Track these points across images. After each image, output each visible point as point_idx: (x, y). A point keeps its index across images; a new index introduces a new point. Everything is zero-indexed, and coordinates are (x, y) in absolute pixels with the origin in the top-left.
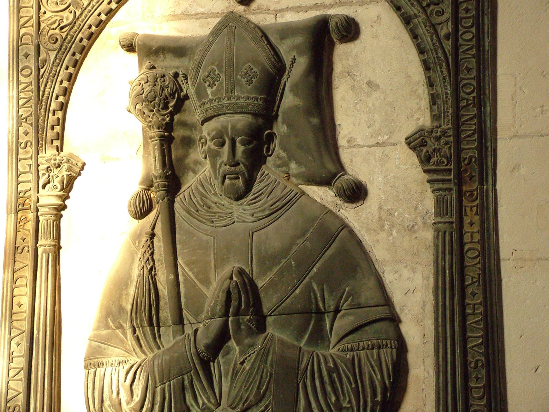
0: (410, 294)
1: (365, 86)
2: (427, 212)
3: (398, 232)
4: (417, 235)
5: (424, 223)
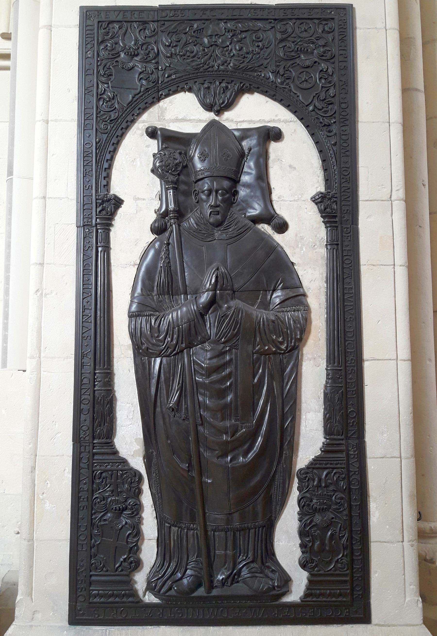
0: (313, 282)
1: (288, 168)
2: (322, 238)
3: (306, 248)
5: (320, 244)
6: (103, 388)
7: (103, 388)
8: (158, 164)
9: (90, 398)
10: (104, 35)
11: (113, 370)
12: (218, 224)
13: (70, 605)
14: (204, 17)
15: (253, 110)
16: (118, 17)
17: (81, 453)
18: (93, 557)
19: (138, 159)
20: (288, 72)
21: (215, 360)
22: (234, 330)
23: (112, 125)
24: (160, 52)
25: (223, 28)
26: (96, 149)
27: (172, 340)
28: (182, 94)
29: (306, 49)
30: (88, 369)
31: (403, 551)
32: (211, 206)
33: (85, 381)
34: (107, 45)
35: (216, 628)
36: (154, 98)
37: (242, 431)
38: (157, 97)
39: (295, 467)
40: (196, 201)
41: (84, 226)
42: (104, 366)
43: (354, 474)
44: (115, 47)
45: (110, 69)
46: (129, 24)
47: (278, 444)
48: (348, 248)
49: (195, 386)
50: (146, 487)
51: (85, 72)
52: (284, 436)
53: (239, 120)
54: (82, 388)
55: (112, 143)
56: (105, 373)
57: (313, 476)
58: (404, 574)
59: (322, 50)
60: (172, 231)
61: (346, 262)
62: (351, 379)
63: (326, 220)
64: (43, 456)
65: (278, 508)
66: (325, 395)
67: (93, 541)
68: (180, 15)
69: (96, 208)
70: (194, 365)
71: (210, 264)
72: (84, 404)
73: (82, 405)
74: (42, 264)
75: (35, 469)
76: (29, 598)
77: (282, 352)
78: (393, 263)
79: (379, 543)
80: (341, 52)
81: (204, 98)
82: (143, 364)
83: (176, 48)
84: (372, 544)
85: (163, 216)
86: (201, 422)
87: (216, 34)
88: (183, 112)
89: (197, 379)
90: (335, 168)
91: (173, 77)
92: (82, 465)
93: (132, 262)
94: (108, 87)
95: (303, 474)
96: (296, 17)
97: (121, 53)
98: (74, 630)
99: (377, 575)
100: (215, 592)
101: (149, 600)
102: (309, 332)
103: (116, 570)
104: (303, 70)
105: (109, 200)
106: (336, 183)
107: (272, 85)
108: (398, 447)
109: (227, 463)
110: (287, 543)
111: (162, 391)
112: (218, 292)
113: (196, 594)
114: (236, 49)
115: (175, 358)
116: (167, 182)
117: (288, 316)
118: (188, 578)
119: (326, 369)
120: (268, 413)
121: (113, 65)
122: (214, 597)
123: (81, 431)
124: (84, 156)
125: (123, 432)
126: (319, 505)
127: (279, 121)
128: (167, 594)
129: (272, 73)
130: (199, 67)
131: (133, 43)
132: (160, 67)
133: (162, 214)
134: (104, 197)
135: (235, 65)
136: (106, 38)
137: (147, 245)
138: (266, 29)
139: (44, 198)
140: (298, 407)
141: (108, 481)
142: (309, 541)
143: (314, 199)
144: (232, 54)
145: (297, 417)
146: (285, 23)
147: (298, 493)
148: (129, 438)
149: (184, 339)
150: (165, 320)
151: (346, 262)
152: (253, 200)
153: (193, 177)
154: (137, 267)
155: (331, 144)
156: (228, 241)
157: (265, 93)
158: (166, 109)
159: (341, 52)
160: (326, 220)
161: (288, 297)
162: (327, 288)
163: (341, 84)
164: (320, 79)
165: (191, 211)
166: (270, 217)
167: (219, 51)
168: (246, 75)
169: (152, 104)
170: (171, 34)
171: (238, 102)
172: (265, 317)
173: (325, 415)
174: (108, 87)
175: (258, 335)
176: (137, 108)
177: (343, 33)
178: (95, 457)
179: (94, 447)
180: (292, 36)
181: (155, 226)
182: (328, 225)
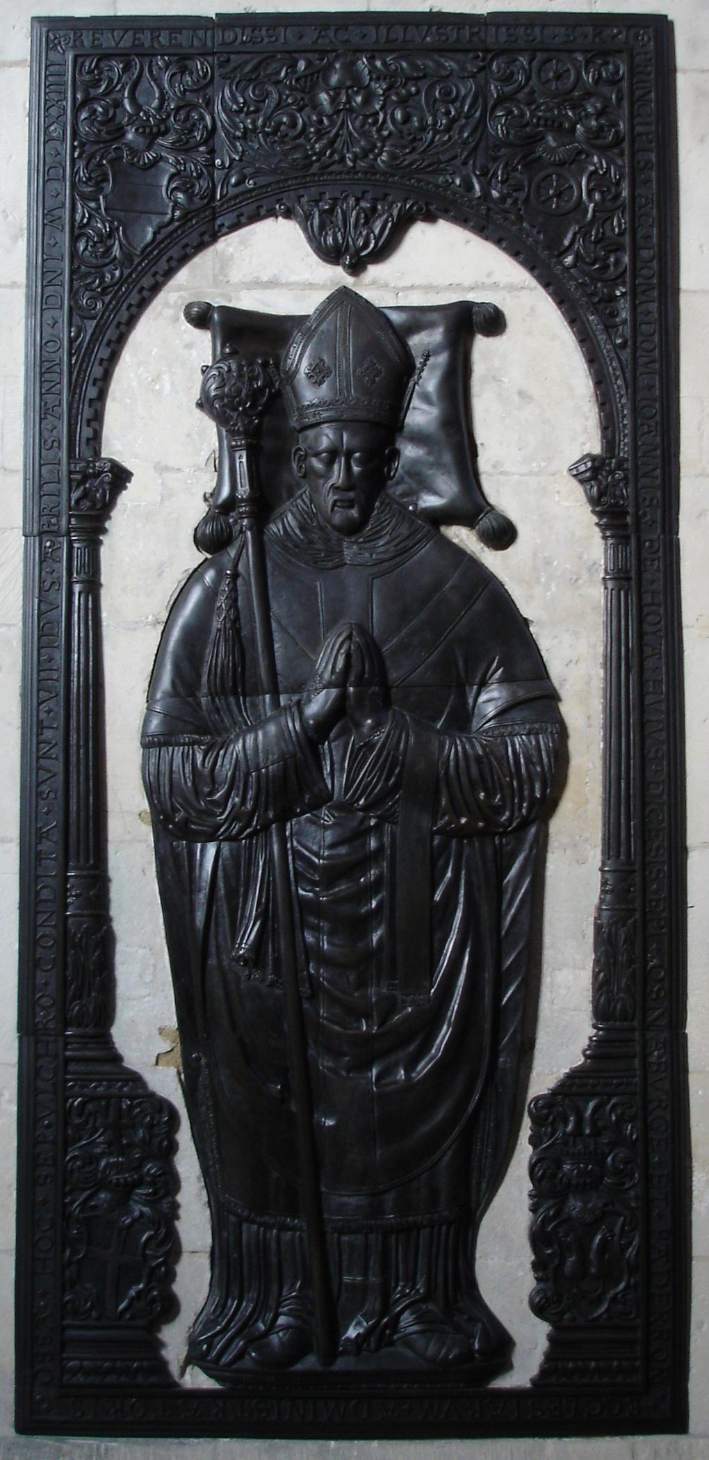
0: (572, 665)
1: (516, 398)
2: (595, 563)
12: (352, 529)
13: (17, 1391)
14: (323, 43)
19: (166, 377)
21: (342, 850)
22: (388, 779)
24: (219, 124)
26: (70, 355)
30: (51, 867)
32: (335, 488)
33: (46, 894)
34: (96, 110)
36: (202, 235)
41: (41, 534)
42: (87, 860)
46: (147, 60)
47: (487, 1040)
49: (296, 909)
50: (184, 1136)
53: (402, 284)
54: (40, 909)
55: (105, 340)
60: (244, 545)
66: (598, 928)
67: (68, 1253)
68: (266, 40)
70: (294, 859)
72: (44, 947)
73: (39, 950)
81: (320, 234)
82: (176, 857)
85: (222, 510)
86: (309, 991)
88: (272, 265)
90: (624, 401)
91: (250, 184)
92: (41, 1084)
93: (150, 618)
95: (543, 1107)
100: (340, 1364)
105: (97, 475)
110: (505, 1258)
115: (251, 843)
116: (232, 433)
120: (464, 971)
123: (38, 1009)
124: (42, 370)
127: (495, 286)
132: (218, 162)
137: (186, 576)
141: (99, 1121)
144: (385, 133)
150: (228, 756)
155: (615, 346)
156: (375, 569)
157: (462, 220)
158: (231, 257)
165: (289, 499)
166: (472, 507)
169: (201, 246)
173: (595, 976)
175: (444, 791)
179: (66, 1044)
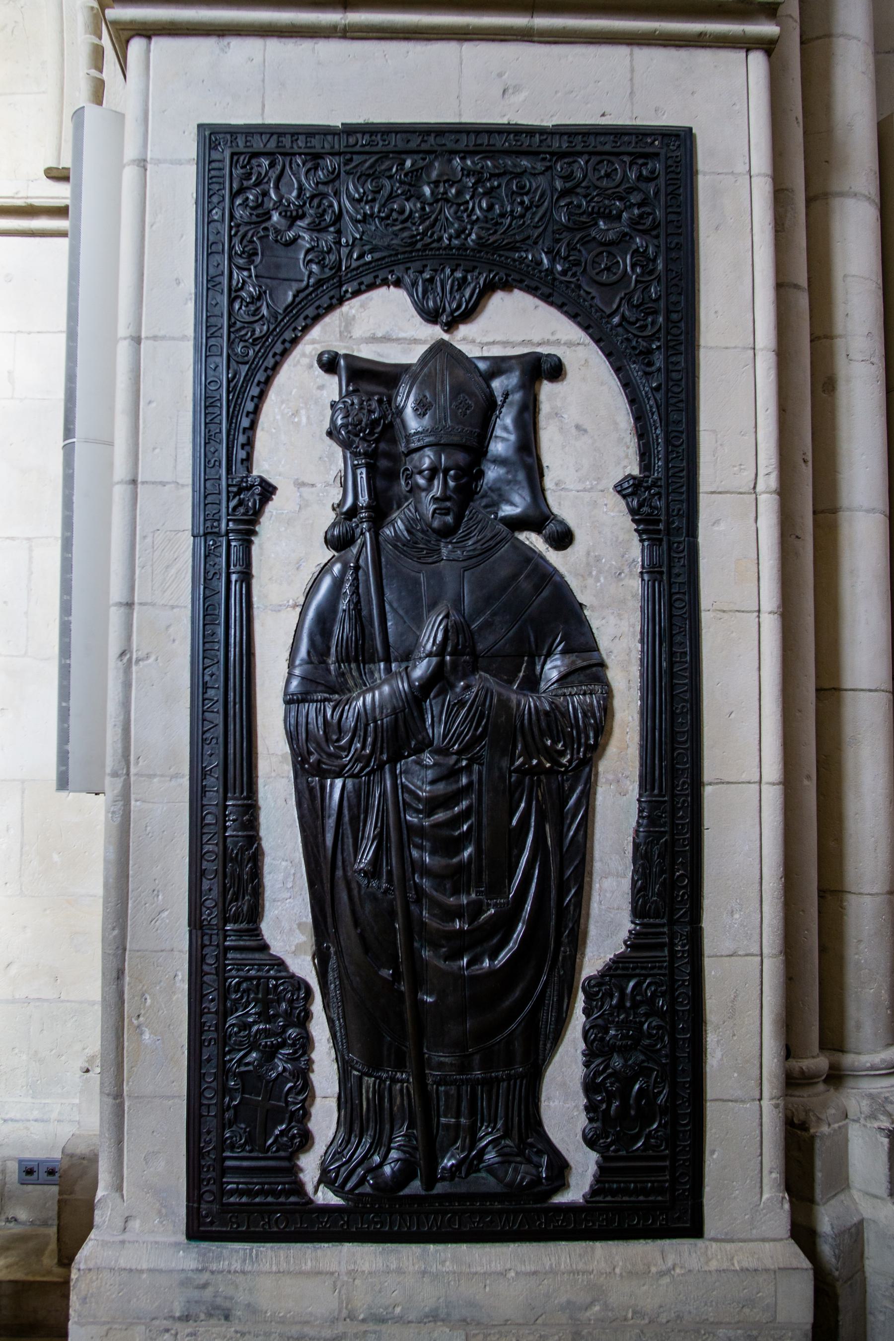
0: (617, 640)
1: (573, 430)
2: (634, 561)
3: (605, 578)
4: (623, 583)
5: (630, 571)
6: (240, 833)
7: (240, 833)
8: (339, 422)
9: (219, 850)
10: (241, 180)
11: (257, 801)
12: (446, 532)
14: (424, 147)
15: (511, 323)
16: (268, 145)
17: (203, 946)
18: (227, 1126)
19: (303, 412)
20: (576, 253)
22: (476, 729)
23: (257, 348)
25: (459, 168)
26: (228, 392)
27: (364, 747)
28: (383, 290)
29: (607, 211)
31: (761, 1115)
32: (435, 499)
33: (210, 819)
34: (247, 198)
35: (440, 1247)
36: (332, 298)
37: (489, 913)
38: (338, 296)
39: (580, 973)
40: (407, 489)
41: (205, 535)
42: (242, 793)
43: (683, 984)
44: (263, 201)
45: (254, 242)
46: (288, 159)
48: (680, 580)
49: (405, 832)
51: (207, 248)
52: (563, 920)
54: (204, 831)
55: (256, 381)
56: (242, 805)
57: (611, 989)
58: (761, 1155)
59: (636, 211)
60: (364, 544)
61: (677, 604)
62: (682, 818)
63: (641, 527)
64: (138, 951)
65: (549, 1045)
66: (636, 846)
67: (227, 1099)
68: (381, 143)
69: (228, 501)
71: (432, 606)
72: (208, 861)
74: (130, 605)
75: (123, 973)
76: (117, 1194)
77: (563, 769)
78: (757, 609)
79: (720, 1103)
80: (672, 217)
81: (423, 298)
82: (311, 790)
83: (372, 204)
84: (708, 1104)
87: (445, 178)
88: (385, 324)
89: (408, 818)
90: (658, 432)
91: (368, 258)
92: (206, 968)
94: (250, 276)
95: (594, 986)
96: (590, 149)
97: (273, 212)
98: (196, 1250)
99: (715, 1156)
100: (440, 1188)
101: (324, 1199)
102: (610, 733)
103: (267, 1152)
104: (601, 249)
105: (250, 488)
106: (659, 460)
107: (546, 276)
108: (758, 937)
109: (461, 968)
111: (346, 840)
112: (448, 658)
113: (406, 1191)
114: (481, 208)
115: (369, 779)
116: (355, 455)
117: (577, 701)
118: (393, 1165)
119: (638, 800)
121: (259, 235)
122: (438, 1196)
123: (204, 909)
124: (206, 404)
125: (276, 912)
126: (621, 1039)
127: (558, 342)
128: (357, 1192)
129: (546, 253)
130: (414, 240)
131: (295, 193)
132: (344, 240)
133: (346, 513)
134: (242, 481)
135: (479, 237)
136: (245, 183)
137: (319, 569)
138: (537, 172)
139: (134, 482)
140: (587, 868)
142: (602, 1101)
143: (619, 489)
144: (474, 217)
145: (586, 887)
146: (571, 160)
147: (583, 1018)
148: (287, 925)
149: (385, 745)
150: (351, 710)
151: (677, 604)
152: (512, 489)
153: (403, 445)
154: (299, 609)
155: (652, 388)
157: (531, 290)
159: (672, 217)
160: (641, 527)
161: (574, 668)
162: (642, 651)
163: (670, 277)
164: (633, 266)
165: (399, 508)
167: (452, 210)
168: (500, 256)
169: (330, 308)
170: (363, 178)
171: (484, 307)
172: (532, 704)
173: (634, 883)
174: (250, 276)
175: (520, 738)
176: (302, 317)
177: (675, 182)
178: (229, 956)
180: (583, 184)
181: (333, 536)
182: (645, 537)
